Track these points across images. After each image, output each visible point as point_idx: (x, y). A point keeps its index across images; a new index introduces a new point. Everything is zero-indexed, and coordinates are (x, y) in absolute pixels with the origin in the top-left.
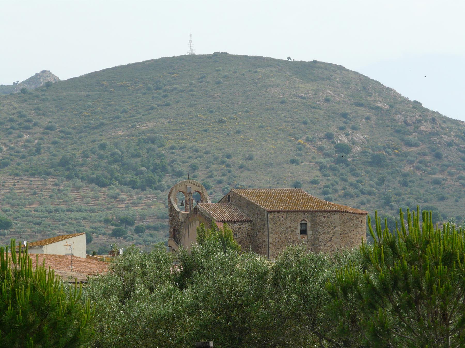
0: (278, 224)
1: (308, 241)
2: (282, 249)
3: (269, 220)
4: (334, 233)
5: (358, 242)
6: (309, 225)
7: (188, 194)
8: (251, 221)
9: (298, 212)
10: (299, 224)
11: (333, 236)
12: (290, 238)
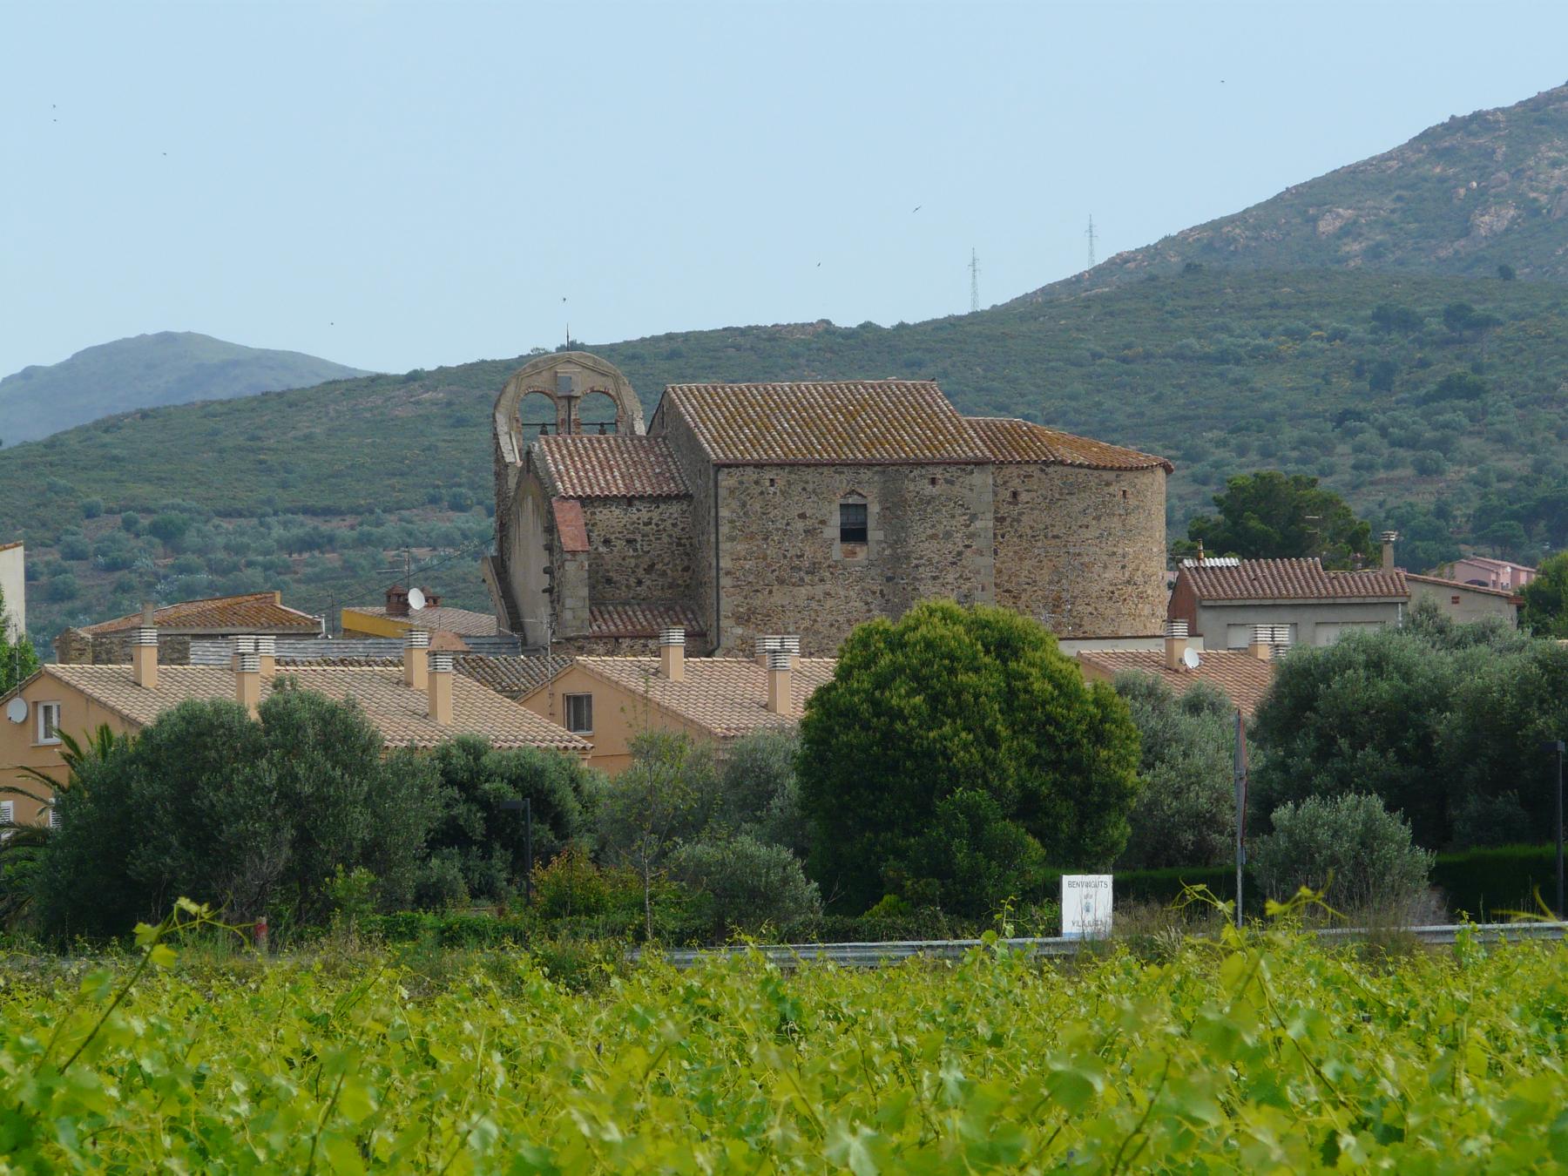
0: (757, 507)
1: (871, 564)
2: (771, 592)
3: (723, 492)
4: (971, 536)
5: (1105, 567)
6: (874, 508)
7: (565, 402)
8: (686, 497)
9: (833, 465)
10: (836, 507)
11: (967, 546)
12: (802, 556)
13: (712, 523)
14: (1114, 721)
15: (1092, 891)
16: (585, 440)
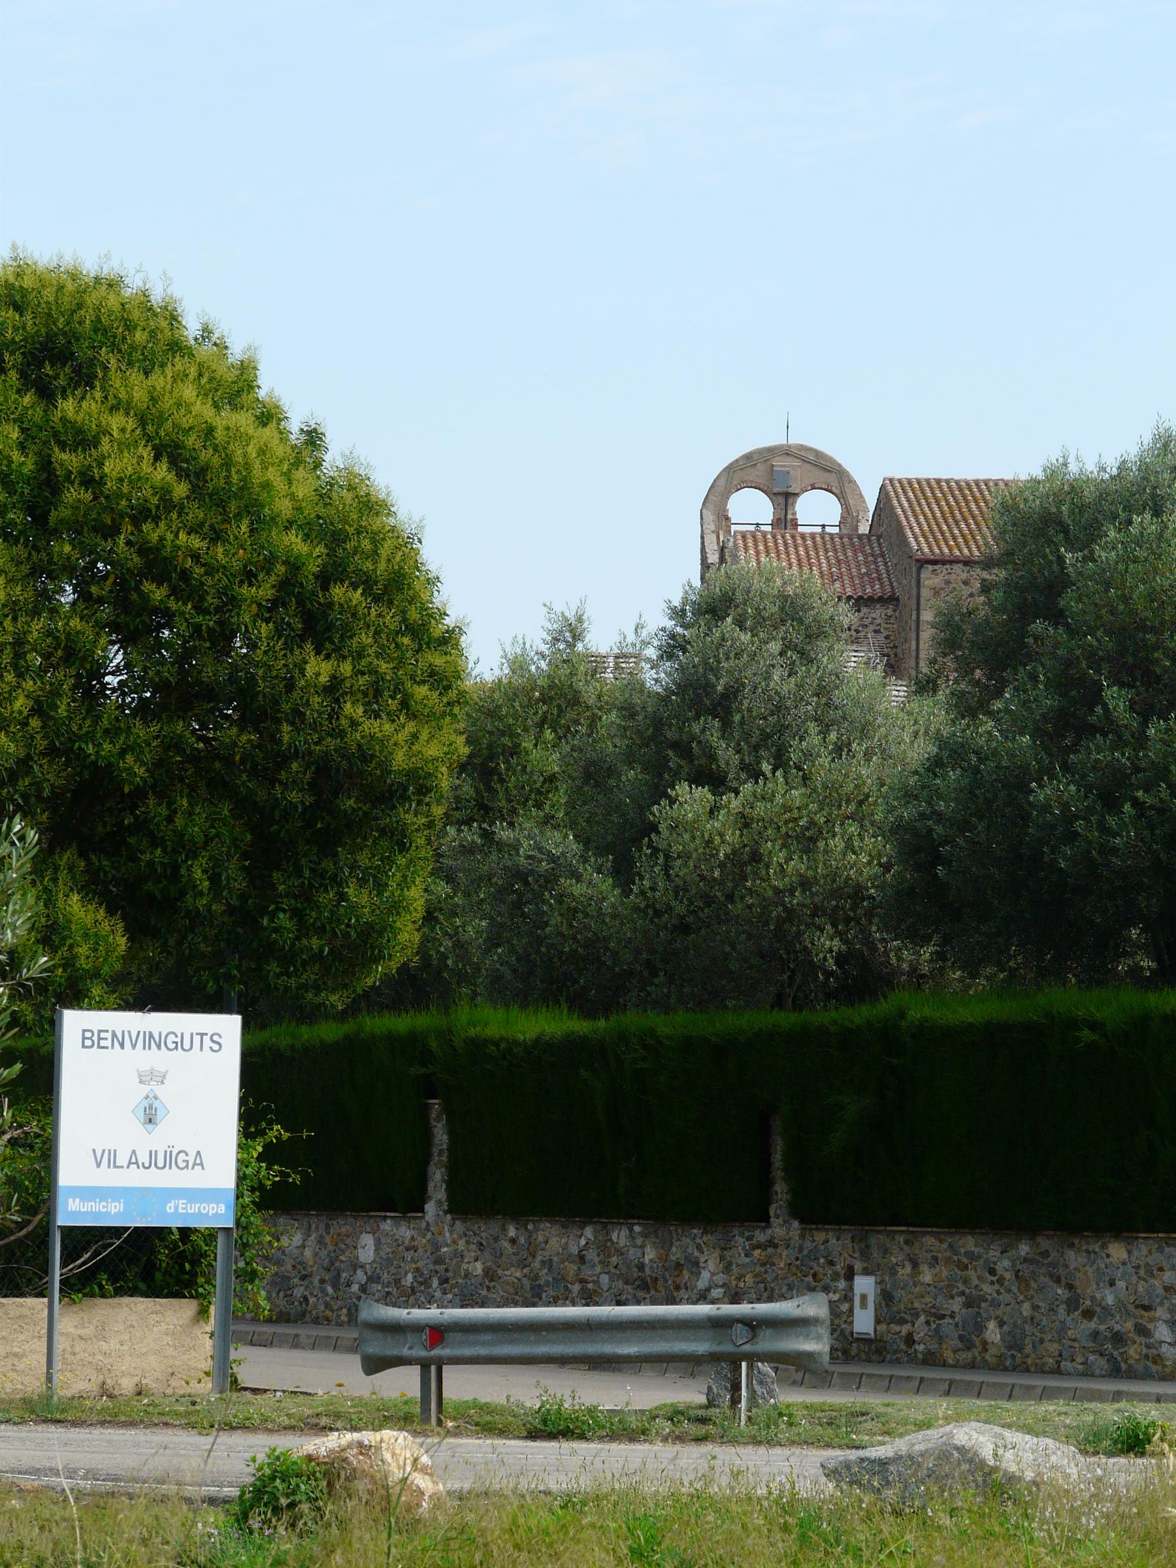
3: (925, 593)
8: (891, 600)
13: (914, 627)
14: (366, 582)
15: (157, 1059)
16: (788, 536)
